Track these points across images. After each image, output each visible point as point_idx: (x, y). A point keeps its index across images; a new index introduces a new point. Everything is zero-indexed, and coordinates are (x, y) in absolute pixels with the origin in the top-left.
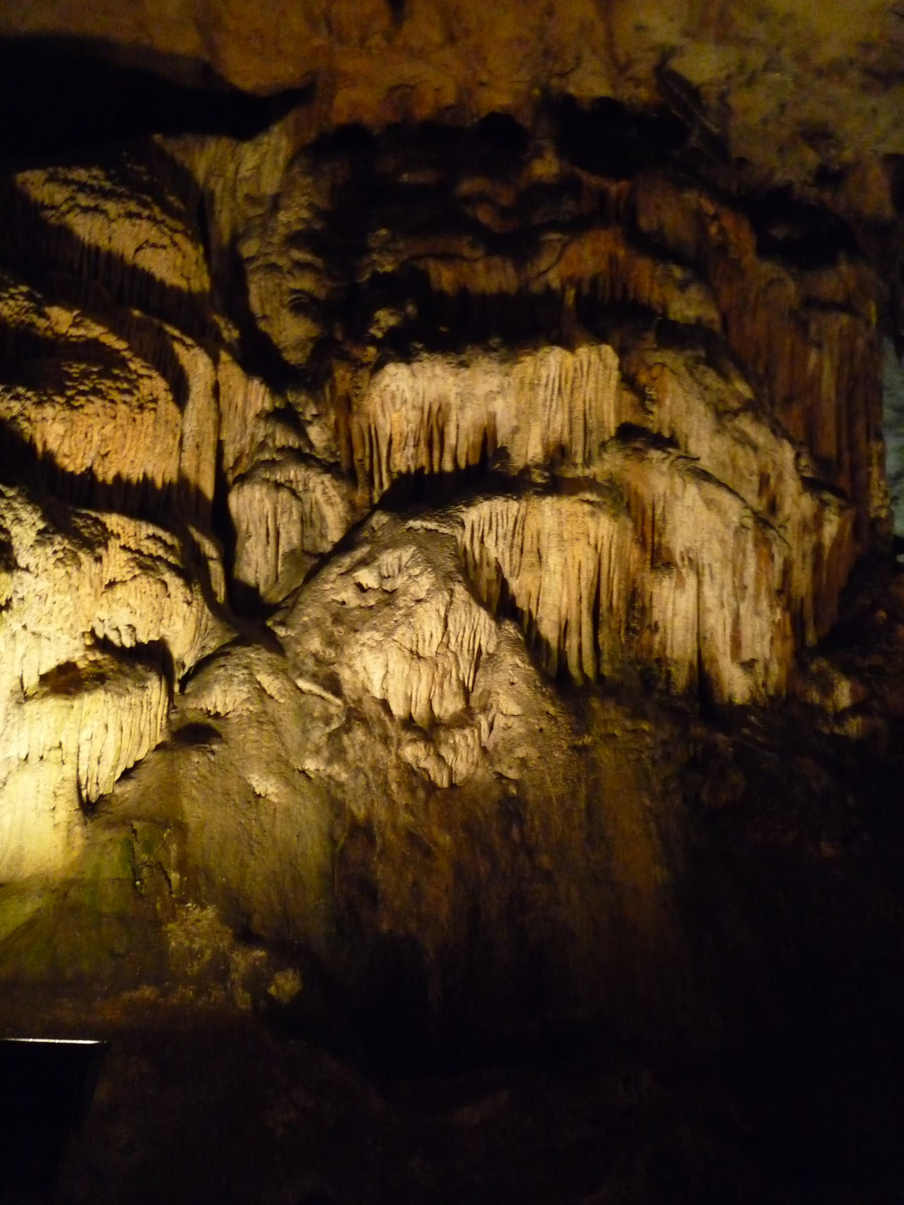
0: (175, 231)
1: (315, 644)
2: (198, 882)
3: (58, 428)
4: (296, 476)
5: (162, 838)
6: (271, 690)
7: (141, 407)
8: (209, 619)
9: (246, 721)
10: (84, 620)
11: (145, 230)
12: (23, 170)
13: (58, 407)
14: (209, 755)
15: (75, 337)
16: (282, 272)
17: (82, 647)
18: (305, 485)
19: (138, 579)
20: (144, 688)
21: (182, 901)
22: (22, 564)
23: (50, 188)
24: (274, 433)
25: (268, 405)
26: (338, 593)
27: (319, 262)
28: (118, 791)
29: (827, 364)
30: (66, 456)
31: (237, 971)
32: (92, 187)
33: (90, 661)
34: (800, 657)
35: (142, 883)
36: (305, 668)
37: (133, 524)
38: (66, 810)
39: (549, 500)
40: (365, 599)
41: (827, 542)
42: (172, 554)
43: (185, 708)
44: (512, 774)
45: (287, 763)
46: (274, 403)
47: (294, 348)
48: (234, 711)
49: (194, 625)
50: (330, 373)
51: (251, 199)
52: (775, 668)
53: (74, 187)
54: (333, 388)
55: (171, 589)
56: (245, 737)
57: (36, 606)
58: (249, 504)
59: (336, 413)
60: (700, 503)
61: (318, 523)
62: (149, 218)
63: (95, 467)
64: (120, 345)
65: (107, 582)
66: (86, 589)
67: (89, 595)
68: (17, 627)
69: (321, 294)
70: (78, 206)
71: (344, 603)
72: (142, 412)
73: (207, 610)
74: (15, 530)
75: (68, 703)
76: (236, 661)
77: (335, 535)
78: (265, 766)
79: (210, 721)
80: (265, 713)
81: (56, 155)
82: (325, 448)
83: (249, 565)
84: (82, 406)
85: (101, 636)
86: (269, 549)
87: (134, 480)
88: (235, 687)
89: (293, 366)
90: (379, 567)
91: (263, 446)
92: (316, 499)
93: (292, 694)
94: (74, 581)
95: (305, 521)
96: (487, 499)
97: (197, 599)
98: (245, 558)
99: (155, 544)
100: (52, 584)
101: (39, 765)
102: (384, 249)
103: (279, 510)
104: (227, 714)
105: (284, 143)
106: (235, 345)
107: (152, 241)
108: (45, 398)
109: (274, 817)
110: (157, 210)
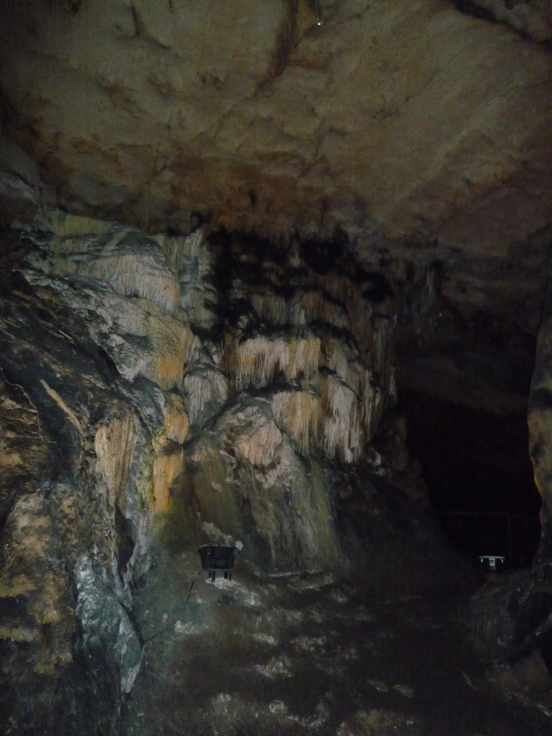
29: (380, 337)
34: (366, 448)
39: (299, 392)
40: (241, 423)
41: (376, 405)
44: (288, 485)
52: (360, 451)
60: (342, 394)
90: (245, 413)
91: (198, 362)
96: (281, 391)
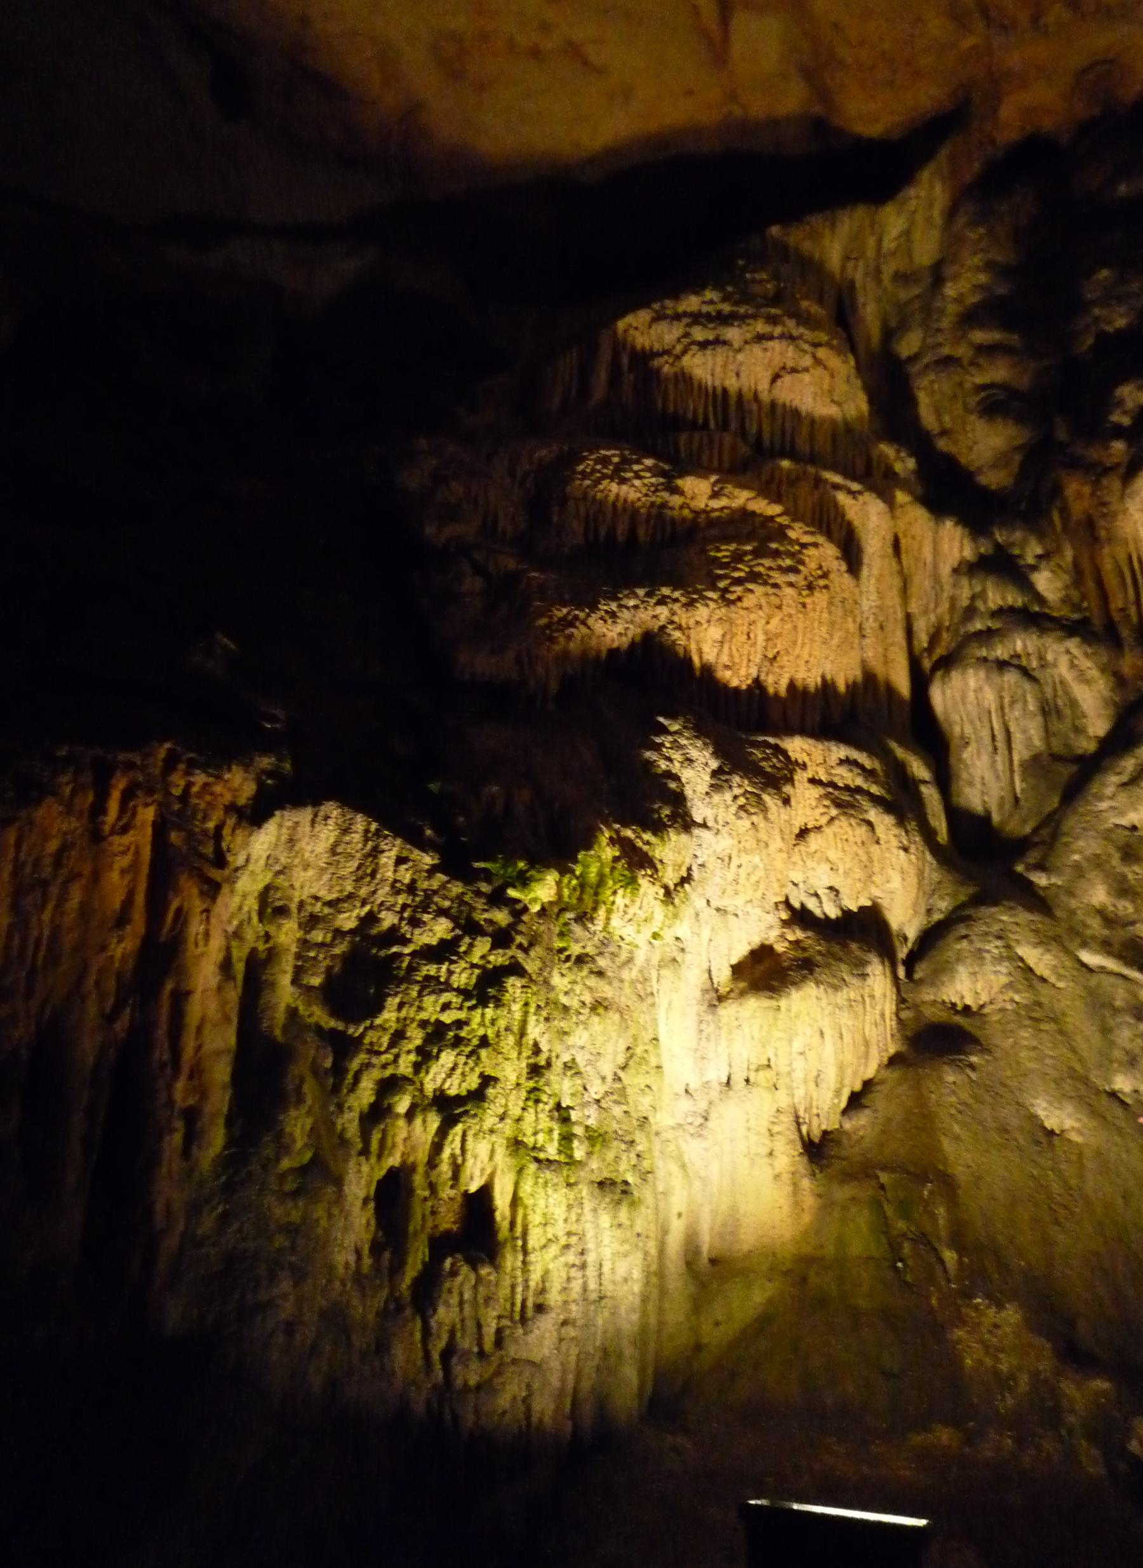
0: (817, 345)
1: (1099, 895)
2: (987, 1268)
3: (715, 632)
4: (1025, 646)
5: (921, 1198)
6: (1041, 970)
7: (810, 587)
8: (933, 872)
9: (1012, 1017)
10: (776, 885)
11: (779, 352)
12: (623, 314)
13: (712, 605)
14: (968, 1071)
15: (716, 510)
16: (962, 367)
17: (777, 923)
18: (1041, 658)
19: (837, 822)
20: (864, 976)
21: (968, 1295)
22: (699, 820)
23: (662, 327)
24: (984, 591)
25: (968, 553)
26: (1122, 814)
27: (1015, 339)
28: (847, 1126)
30: (727, 667)
31: (1072, 1411)
32: (708, 316)
33: (790, 942)
35: (905, 1265)
36: (1089, 932)
37: (820, 746)
38: (788, 1156)
42: (875, 783)
43: (918, 1001)
45: (1085, 1081)
46: (977, 548)
47: (994, 466)
48: (991, 1003)
49: (916, 880)
50: (1057, 491)
51: (901, 278)
53: (686, 320)
54: (1065, 511)
55: (880, 830)
56: (1015, 1043)
57: (718, 873)
58: (964, 699)
59: (1074, 548)
61: (1067, 711)
62: (782, 336)
63: (763, 677)
64: (774, 509)
65: (797, 831)
66: (776, 844)
67: (780, 851)
68: (700, 903)
69: (1024, 382)
70: (694, 343)
71: (1134, 828)
72: (812, 594)
73: (929, 857)
74: (686, 774)
75: (774, 1003)
76: (984, 928)
77: (1098, 726)
78: (1053, 1085)
79: (958, 1019)
80: (1039, 1004)
81: (656, 284)
82: (1063, 601)
83: (971, 784)
84: (740, 599)
85: (797, 905)
86: (998, 758)
87: (812, 689)
88: (989, 968)
89: (994, 492)
91: (970, 612)
92: (1060, 675)
93: (1075, 973)
94: (763, 835)
95: (1048, 710)
97: (915, 842)
98: (965, 775)
99: (851, 771)
100: (735, 842)
101: (745, 1092)
102: (1110, 297)
103: (1007, 700)
104: (982, 1007)
105: (938, 189)
106: (913, 477)
107: (790, 364)
108: (695, 596)
109: (1081, 1166)
110: (791, 323)
